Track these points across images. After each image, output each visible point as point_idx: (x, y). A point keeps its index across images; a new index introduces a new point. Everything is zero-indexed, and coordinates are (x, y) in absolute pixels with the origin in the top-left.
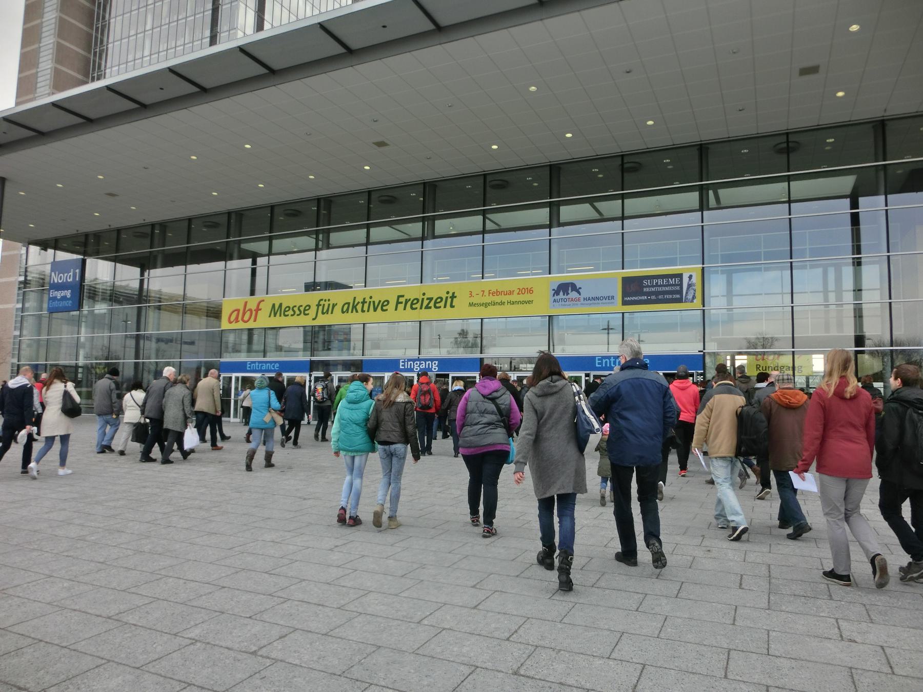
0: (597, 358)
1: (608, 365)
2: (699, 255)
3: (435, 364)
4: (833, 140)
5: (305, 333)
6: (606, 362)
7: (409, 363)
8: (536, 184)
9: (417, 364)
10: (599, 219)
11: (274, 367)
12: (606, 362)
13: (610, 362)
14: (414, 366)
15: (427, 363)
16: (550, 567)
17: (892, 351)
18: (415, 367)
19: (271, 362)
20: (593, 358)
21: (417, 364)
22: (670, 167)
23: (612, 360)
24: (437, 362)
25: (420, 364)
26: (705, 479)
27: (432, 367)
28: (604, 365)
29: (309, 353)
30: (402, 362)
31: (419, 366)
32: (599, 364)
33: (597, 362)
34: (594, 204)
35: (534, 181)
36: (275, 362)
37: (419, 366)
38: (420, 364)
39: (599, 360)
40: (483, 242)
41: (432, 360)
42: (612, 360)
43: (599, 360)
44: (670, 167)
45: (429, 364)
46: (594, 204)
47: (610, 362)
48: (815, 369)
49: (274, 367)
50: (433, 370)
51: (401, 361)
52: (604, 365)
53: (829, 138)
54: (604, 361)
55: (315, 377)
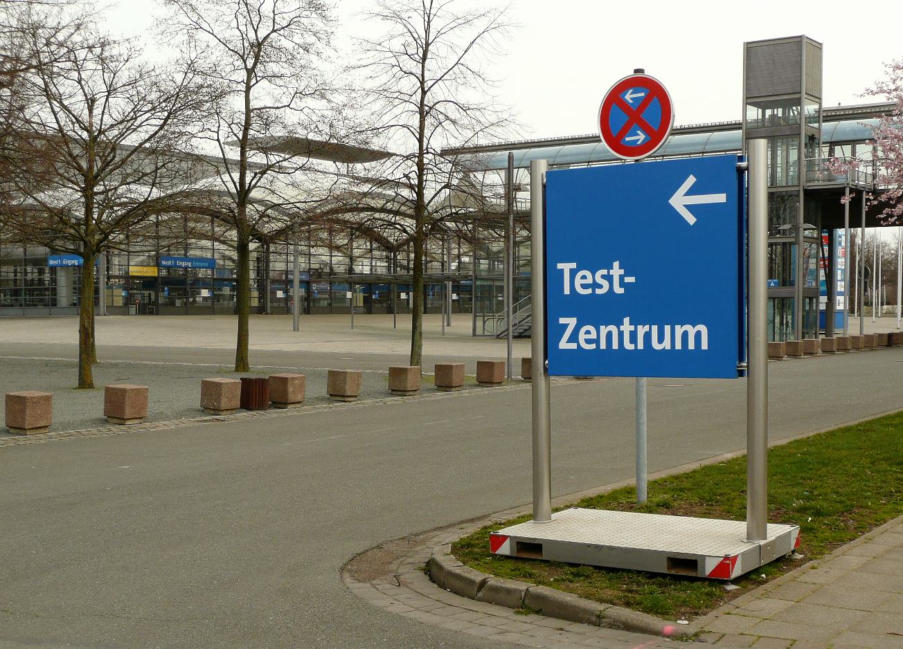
12: (609, 335)
13: (621, 334)
47: (621, 334)
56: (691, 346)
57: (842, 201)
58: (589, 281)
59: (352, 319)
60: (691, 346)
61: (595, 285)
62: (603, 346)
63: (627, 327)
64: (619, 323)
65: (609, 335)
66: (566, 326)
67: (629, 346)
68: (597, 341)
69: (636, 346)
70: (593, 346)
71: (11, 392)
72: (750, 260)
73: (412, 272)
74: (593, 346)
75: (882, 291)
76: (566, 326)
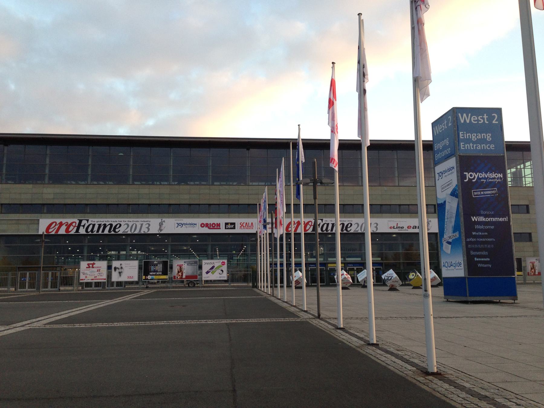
2: (321, 297)
3: (489, 135)
5: (296, 139)
7: (468, 135)
9: (474, 135)
10: (361, 19)
12: (467, 146)
13: (470, 146)
14: (486, 137)
16: (436, 213)
17: (242, 241)
18: (488, 138)
25: (477, 135)
26: (517, 301)
27: (472, 138)
31: (476, 137)
37: (476, 137)
38: (477, 135)
40: (237, 262)
45: (484, 136)
47: (470, 146)
52: (466, 148)
56: (492, 221)
57: (451, 124)
58: (476, 119)
59: (130, 148)
60: (492, 221)
61: (478, 120)
62: (465, 138)
63: (471, 145)
64: (469, 144)
65: (467, 146)
66: (450, 118)
67: (472, 148)
68: (465, 148)
69: (474, 148)
70: (463, 138)
71: (397, 279)
72: (452, 303)
73: (525, 186)
74: (463, 138)
75: (72, 264)
76: (450, 118)
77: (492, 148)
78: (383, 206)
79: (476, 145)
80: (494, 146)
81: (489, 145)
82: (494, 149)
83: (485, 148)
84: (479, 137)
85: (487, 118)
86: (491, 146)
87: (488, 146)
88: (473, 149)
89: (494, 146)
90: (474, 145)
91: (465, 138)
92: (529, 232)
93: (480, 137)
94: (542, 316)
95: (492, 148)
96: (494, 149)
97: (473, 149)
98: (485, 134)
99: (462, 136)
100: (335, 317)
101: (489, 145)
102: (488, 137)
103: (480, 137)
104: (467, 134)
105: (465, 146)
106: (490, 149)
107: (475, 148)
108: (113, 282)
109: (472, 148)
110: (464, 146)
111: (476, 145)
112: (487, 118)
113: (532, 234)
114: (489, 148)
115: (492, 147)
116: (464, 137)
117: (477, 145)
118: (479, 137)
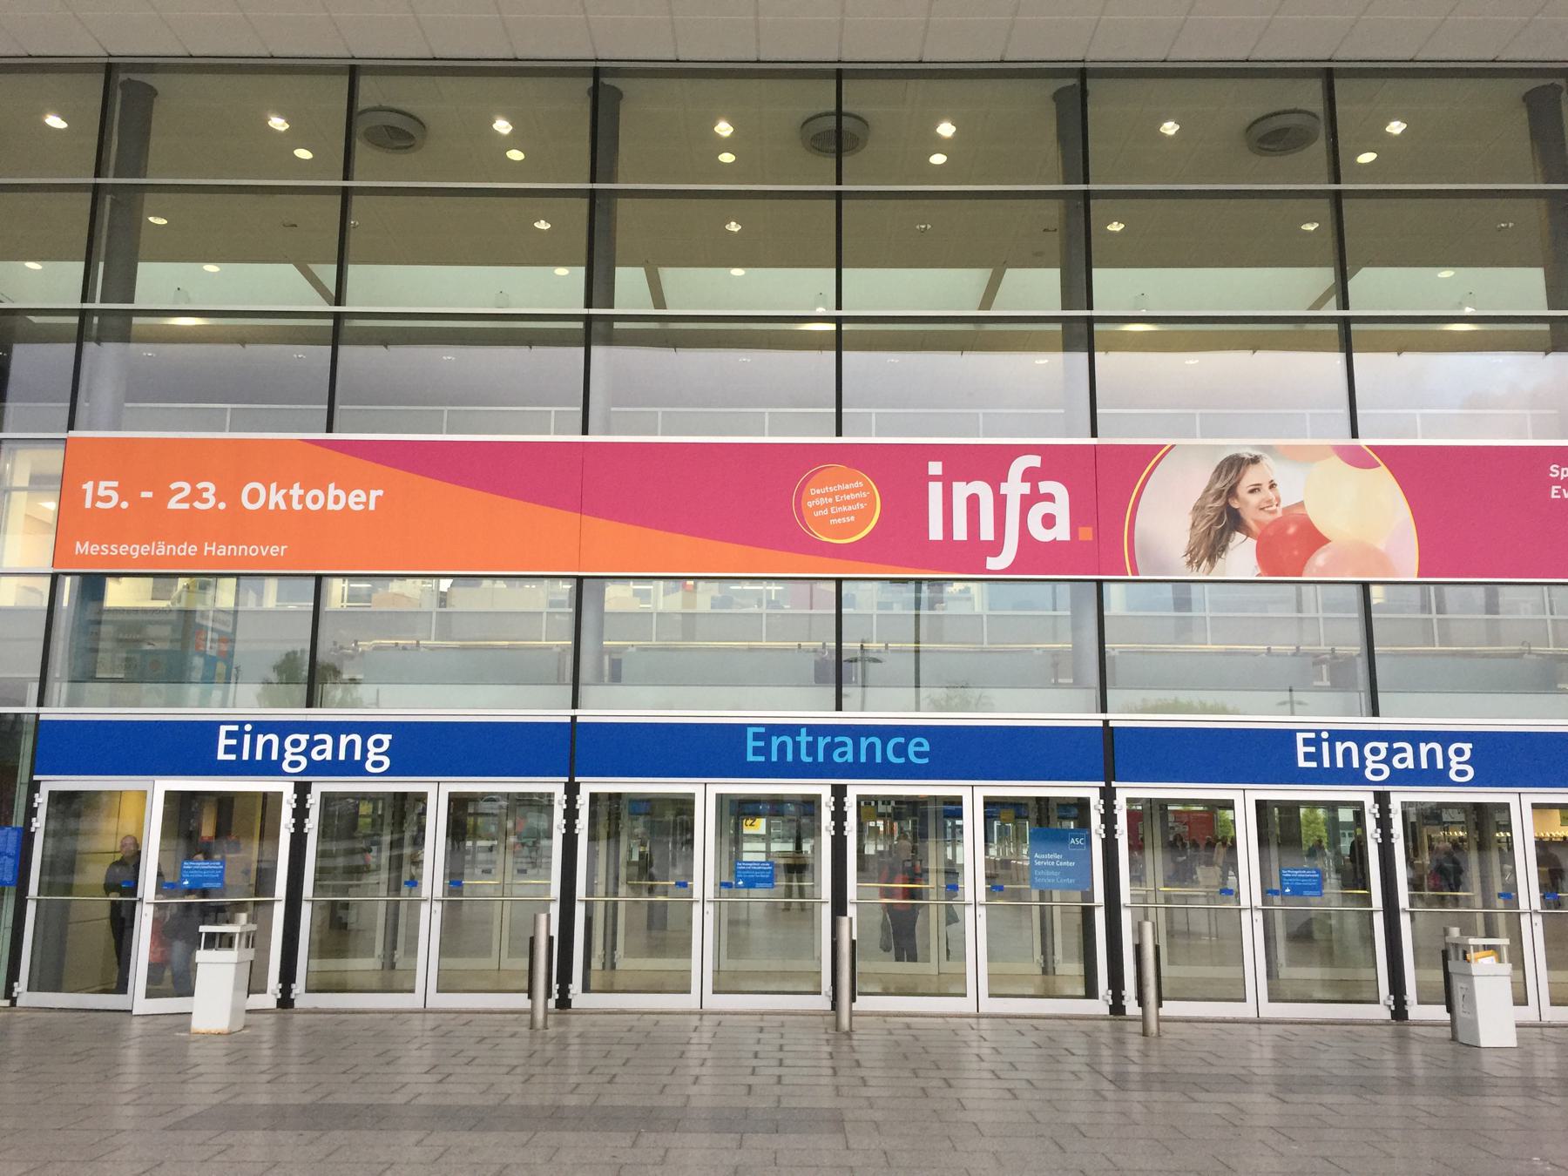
0: (750, 731)
1: (790, 757)
3: (1459, 752)
4: (165, 222)
6: (783, 746)
7: (261, 740)
8: (303, 154)
9: (296, 743)
11: (901, 750)
12: (783, 746)
13: (797, 745)
15: (344, 740)
19: (885, 732)
20: (736, 732)
21: (296, 743)
22: (727, 158)
23: (804, 739)
24: (1467, 747)
28: (774, 758)
29: (301, 691)
30: (229, 735)
31: (1388, 761)
32: (756, 751)
33: (751, 744)
34: (311, 266)
35: (297, 136)
36: (909, 732)
37: (1388, 761)
39: (757, 737)
41: (366, 729)
42: (804, 739)
43: (757, 737)
44: (727, 158)
46: (311, 266)
47: (797, 745)
48: (788, 760)
49: (901, 750)
50: (1453, 776)
51: (223, 729)
52: (774, 758)
53: (156, 215)
54: (775, 741)
55: (860, 798)
62: (1326, 764)
69: (815, 758)
77: (918, 754)
78: (1521, 972)
79: (828, 739)
80: (926, 748)
81: (902, 740)
82: (926, 761)
83: (878, 759)
84: (1402, 761)
85: (807, 742)
86: (912, 749)
87: (896, 745)
88: (810, 760)
89: (926, 748)
90: (820, 739)
91: (1326, 764)
92: (587, 995)
93: (1410, 764)
94: (1500, 1082)
95: (918, 754)
96: (926, 761)
97: (810, 760)
98: (234, 547)
99: (1308, 757)
100: (1296, 1032)
101: (902, 740)
102: (1453, 764)
103: (1410, 764)
104: (1338, 744)
105: (768, 744)
106: (902, 760)
107: (821, 758)
108: (202, 933)
109: (808, 754)
110: (761, 744)
111: (828, 739)
112: (807, 742)
113: (412, 994)
114: (897, 754)
115: (918, 749)
116: (1320, 762)
117: (838, 739)
118: (1402, 761)
